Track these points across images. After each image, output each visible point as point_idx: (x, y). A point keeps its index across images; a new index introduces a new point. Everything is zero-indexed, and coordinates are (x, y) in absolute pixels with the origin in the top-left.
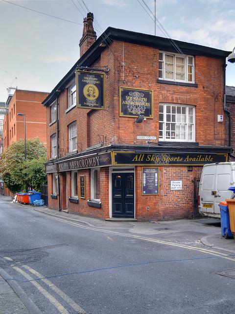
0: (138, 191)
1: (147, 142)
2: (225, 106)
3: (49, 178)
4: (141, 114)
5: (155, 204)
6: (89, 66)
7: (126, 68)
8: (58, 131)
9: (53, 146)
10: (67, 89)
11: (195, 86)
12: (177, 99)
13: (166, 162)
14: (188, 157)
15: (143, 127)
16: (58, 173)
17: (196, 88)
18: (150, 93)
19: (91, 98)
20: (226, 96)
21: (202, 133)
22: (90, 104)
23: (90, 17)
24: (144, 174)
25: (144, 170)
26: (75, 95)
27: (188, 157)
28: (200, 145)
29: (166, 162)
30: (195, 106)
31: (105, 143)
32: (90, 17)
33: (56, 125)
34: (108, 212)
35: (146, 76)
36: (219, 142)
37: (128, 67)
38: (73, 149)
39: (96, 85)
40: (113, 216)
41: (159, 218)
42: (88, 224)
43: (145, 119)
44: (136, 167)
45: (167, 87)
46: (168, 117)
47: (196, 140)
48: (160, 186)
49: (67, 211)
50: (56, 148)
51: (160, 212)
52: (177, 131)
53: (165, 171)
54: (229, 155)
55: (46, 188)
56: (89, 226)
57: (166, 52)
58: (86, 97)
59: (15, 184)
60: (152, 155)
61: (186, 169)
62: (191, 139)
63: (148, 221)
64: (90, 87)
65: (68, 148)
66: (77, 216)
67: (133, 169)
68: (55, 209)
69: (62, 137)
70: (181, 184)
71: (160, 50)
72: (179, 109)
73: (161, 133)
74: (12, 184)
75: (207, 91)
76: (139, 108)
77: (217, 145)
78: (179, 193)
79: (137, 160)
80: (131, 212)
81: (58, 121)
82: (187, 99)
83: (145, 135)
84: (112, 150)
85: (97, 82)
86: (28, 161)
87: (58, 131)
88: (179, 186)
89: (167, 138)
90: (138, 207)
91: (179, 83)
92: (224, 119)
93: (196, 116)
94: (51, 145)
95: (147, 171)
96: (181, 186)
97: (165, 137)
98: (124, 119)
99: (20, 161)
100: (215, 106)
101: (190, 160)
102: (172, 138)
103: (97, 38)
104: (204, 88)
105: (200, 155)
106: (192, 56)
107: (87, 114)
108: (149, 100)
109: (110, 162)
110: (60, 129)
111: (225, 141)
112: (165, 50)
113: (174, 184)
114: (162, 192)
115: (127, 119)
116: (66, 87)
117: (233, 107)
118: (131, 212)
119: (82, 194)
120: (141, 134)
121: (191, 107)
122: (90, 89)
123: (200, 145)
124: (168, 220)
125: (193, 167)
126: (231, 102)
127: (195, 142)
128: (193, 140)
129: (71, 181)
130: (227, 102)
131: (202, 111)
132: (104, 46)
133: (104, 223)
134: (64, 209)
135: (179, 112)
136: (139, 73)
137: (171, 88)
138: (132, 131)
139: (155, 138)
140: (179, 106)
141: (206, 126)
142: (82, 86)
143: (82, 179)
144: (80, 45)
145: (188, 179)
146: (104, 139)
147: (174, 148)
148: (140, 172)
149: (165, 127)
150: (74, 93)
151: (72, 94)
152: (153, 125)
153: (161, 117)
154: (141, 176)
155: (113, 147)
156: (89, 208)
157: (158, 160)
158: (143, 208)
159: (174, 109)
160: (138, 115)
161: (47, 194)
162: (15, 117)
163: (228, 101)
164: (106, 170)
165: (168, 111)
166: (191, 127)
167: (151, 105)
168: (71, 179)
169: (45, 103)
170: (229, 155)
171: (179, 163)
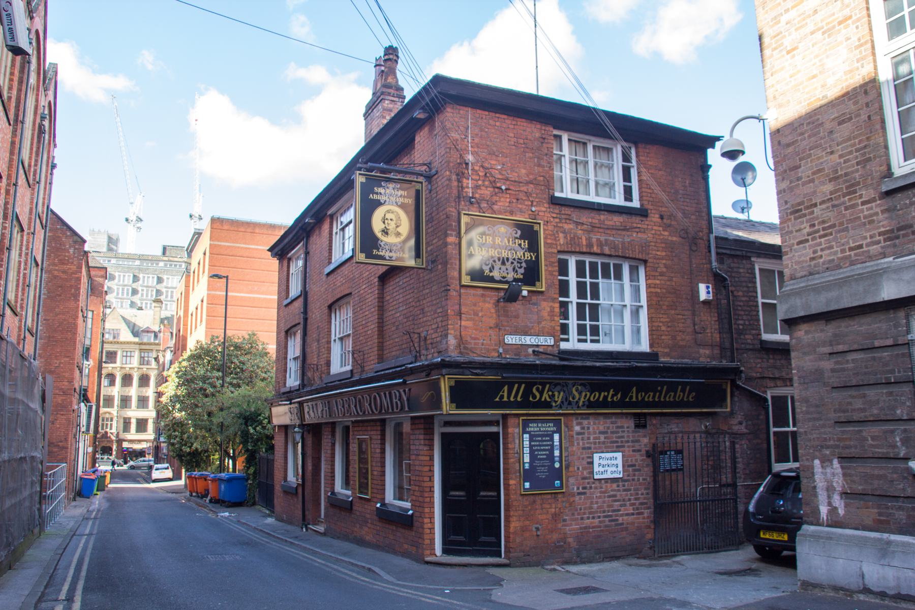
1: (530, 350)
2: (714, 264)
3: (278, 441)
4: (515, 280)
5: (556, 517)
6: (387, 163)
7: (477, 168)
8: (306, 320)
9: (290, 356)
10: (332, 217)
11: (642, 213)
12: (600, 244)
13: (581, 403)
14: (634, 389)
15: (521, 312)
17: (644, 219)
18: (536, 228)
19: (391, 239)
20: (716, 238)
21: (663, 328)
22: (387, 255)
23: (391, 55)
24: (526, 436)
25: (526, 424)
26: (349, 231)
27: (634, 389)
28: (662, 359)
29: (581, 403)
31: (424, 352)
32: (391, 55)
33: (299, 304)
34: (432, 540)
35: (524, 189)
36: (707, 352)
37: (482, 166)
38: (339, 365)
39: (402, 206)
40: (445, 551)
41: (566, 555)
43: (525, 293)
44: (505, 417)
45: (575, 215)
46: (581, 287)
47: (651, 346)
48: (567, 467)
49: (321, 528)
50: (299, 362)
51: (570, 540)
55: (270, 463)
57: (570, 133)
59: (194, 448)
61: (629, 423)
62: (639, 342)
63: (538, 564)
64: (388, 211)
65: (328, 364)
66: (347, 546)
67: (497, 423)
68: (290, 522)
69: (313, 334)
70: (619, 461)
71: (555, 128)
72: (606, 267)
73: (564, 329)
74: (188, 450)
76: (508, 264)
77: (701, 360)
78: (615, 486)
79: (505, 399)
80: (493, 539)
81: (305, 294)
83: (526, 334)
85: (406, 201)
87: (306, 320)
88: (614, 469)
91: (605, 205)
92: (715, 294)
93: (648, 286)
94: (286, 353)
96: (620, 468)
97: (576, 337)
98: (472, 291)
100: (691, 262)
101: (640, 398)
102: (592, 341)
103: (406, 101)
104: (662, 217)
105: (662, 384)
106: (631, 145)
108: (533, 246)
109: (437, 404)
110: (310, 314)
113: (603, 462)
114: (573, 485)
115: (480, 292)
116: (329, 213)
117: (732, 265)
118: (493, 539)
120: (516, 332)
121: (634, 263)
122: (389, 216)
123: (662, 359)
125: (648, 418)
126: (728, 252)
128: (644, 346)
130: (717, 254)
131: (662, 274)
132: (422, 116)
133: (415, 566)
135: (606, 275)
136: (507, 179)
137: (586, 218)
138: (492, 322)
139: (550, 341)
141: (673, 312)
142: (369, 207)
143: (364, 446)
144: (366, 115)
145: (637, 448)
146: (422, 343)
147: (599, 367)
148: (514, 430)
149: (573, 311)
150: (347, 225)
151: (343, 229)
152: (546, 307)
153: (564, 289)
154: (517, 441)
155: (444, 365)
157: (559, 397)
158: (524, 529)
159: (593, 266)
160: (507, 282)
161: (273, 479)
162: (204, 279)
164: (427, 424)
165: (580, 272)
166: (636, 312)
167: (537, 257)
168: (333, 445)
169: (276, 250)
171: (613, 405)
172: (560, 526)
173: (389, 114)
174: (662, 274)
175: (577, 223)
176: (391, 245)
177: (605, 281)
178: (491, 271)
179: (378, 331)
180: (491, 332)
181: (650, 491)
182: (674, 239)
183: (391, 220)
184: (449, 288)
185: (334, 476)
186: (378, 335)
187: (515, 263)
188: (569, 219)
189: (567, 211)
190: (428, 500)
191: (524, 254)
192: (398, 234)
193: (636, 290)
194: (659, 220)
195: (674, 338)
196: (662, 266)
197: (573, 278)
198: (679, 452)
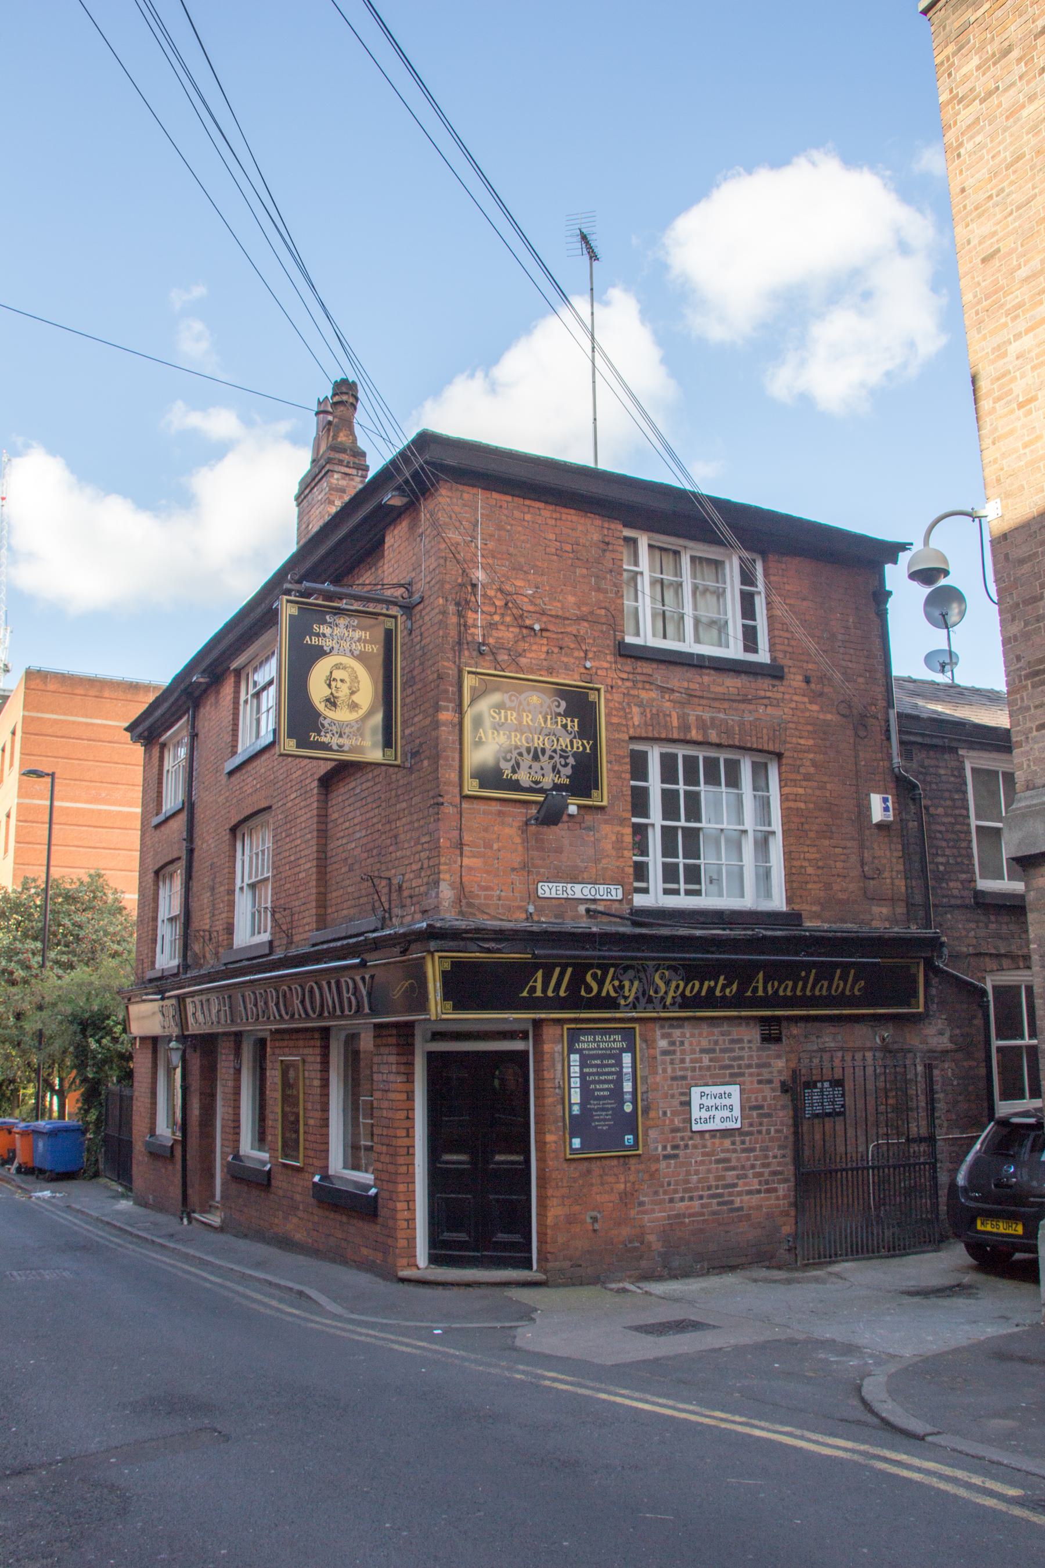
0: (550, 1138)
1: (582, 909)
2: (897, 760)
3: (141, 1064)
4: (557, 787)
5: (627, 1198)
6: (337, 581)
7: (491, 593)
8: (191, 852)
9: (163, 914)
10: (238, 673)
11: (774, 672)
12: (702, 726)
13: (669, 1001)
14: (761, 975)
15: (566, 842)
16: (183, 1038)
17: (777, 683)
18: (593, 696)
20: (900, 716)
21: (810, 870)
22: (335, 741)
24: (575, 1058)
25: (574, 1037)
26: (269, 698)
27: (761, 975)
28: (808, 924)
29: (669, 1001)
30: (779, 756)
31: (397, 911)
33: (179, 824)
35: (573, 629)
36: (885, 910)
37: (500, 590)
40: (435, 1260)
42: (322, 1299)
43: (573, 809)
44: (537, 1024)
45: (659, 674)
46: (669, 800)
47: (789, 900)
48: (646, 1111)
51: (651, 1238)
52: (706, 860)
53: (663, 1044)
54: (931, 968)
55: (125, 1104)
56: (322, 1311)
57: (651, 534)
58: (321, 707)
60: (605, 969)
61: (752, 1034)
62: (768, 894)
63: (595, 1280)
64: (337, 666)
65: (230, 929)
66: (261, 1250)
70: (735, 1100)
71: (625, 526)
72: (712, 765)
73: (641, 871)
75: (821, 694)
77: (875, 924)
80: (516, 1238)
81: (189, 807)
82: (742, 724)
84: (433, 945)
85: (369, 648)
86: (51, 974)
87: (191, 852)
88: (726, 1113)
89: (666, 892)
90: (551, 1214)
92: (899, 811)
93: (784, 798)
95: (586, 1043)
96: (737, 1112)
97: (661, 885)
98: (482, 806)
99: (20, 973)
100: (856, 757)
102: (688, 893)
103: (371, 474)
104: (807, 680)
105: (808, 966)
106: (755, 556)
107: (320, 780)
110: (198, 842)
111: (910, 905)
112: (648, 528)
114: (655, 1140)
115: (495, 807)
116: (234, 666)
117: (927, 762)
118: (516, 1238)
119: (290, 1147)
121: (760, 758)
122: (338, 674)
123: (808, 924)
124: (685, 1274)
125: (784, 1024)
127: (784, 908)
128: (778, 902)
129: (237, 1079)
130: (902, 743)
131: (807, 778)
134: (203, 1212)
135: (713, 779)
136: (543, 613)
137: (678, 679)
138: (516, 859)
140: (712, 754)
141: (827, 842)
144: (300, 498)
145: (766, 1076)
146: (394, 896)
148: (554, 1046)
149: (655, 840)
150: (265, 688)
151: (257, 695)
153: (639, 802)
155: (433, 934)
156: (158, 831)
158: (571, 1220)
159: (691, 763)
160: (541, 791)
163: (906, 738)
165: (668, 774)
166: (763, 843)
167: (595, 748)
168: (238, 1071)
169: (140, 729)
170: (931, 968)
171: (725, 1003)
172: (633, 1213)
173: (341, 497)
174: (807, 778)
175: (663, 690)
176: (341, 724)
177: (710, 788)
178: (514, 772)
179: (318, 873)
180: (514, 876)
181: (789, 1152)
182: (829, 717)
183: (342, 681)
184: (441, 800)
185: (239, 1127)
186: (318, 880)
187: (557, 757)
188: (648, 682)
189: (646, 668)
190: (403, 1169)
191: (571, 742)
192: (354, 706)
193: (764, 805)
194: (803, 685)
195: (828, 886)
196: (808, 763)
197: (655, 785)
198: (838, 1083)
